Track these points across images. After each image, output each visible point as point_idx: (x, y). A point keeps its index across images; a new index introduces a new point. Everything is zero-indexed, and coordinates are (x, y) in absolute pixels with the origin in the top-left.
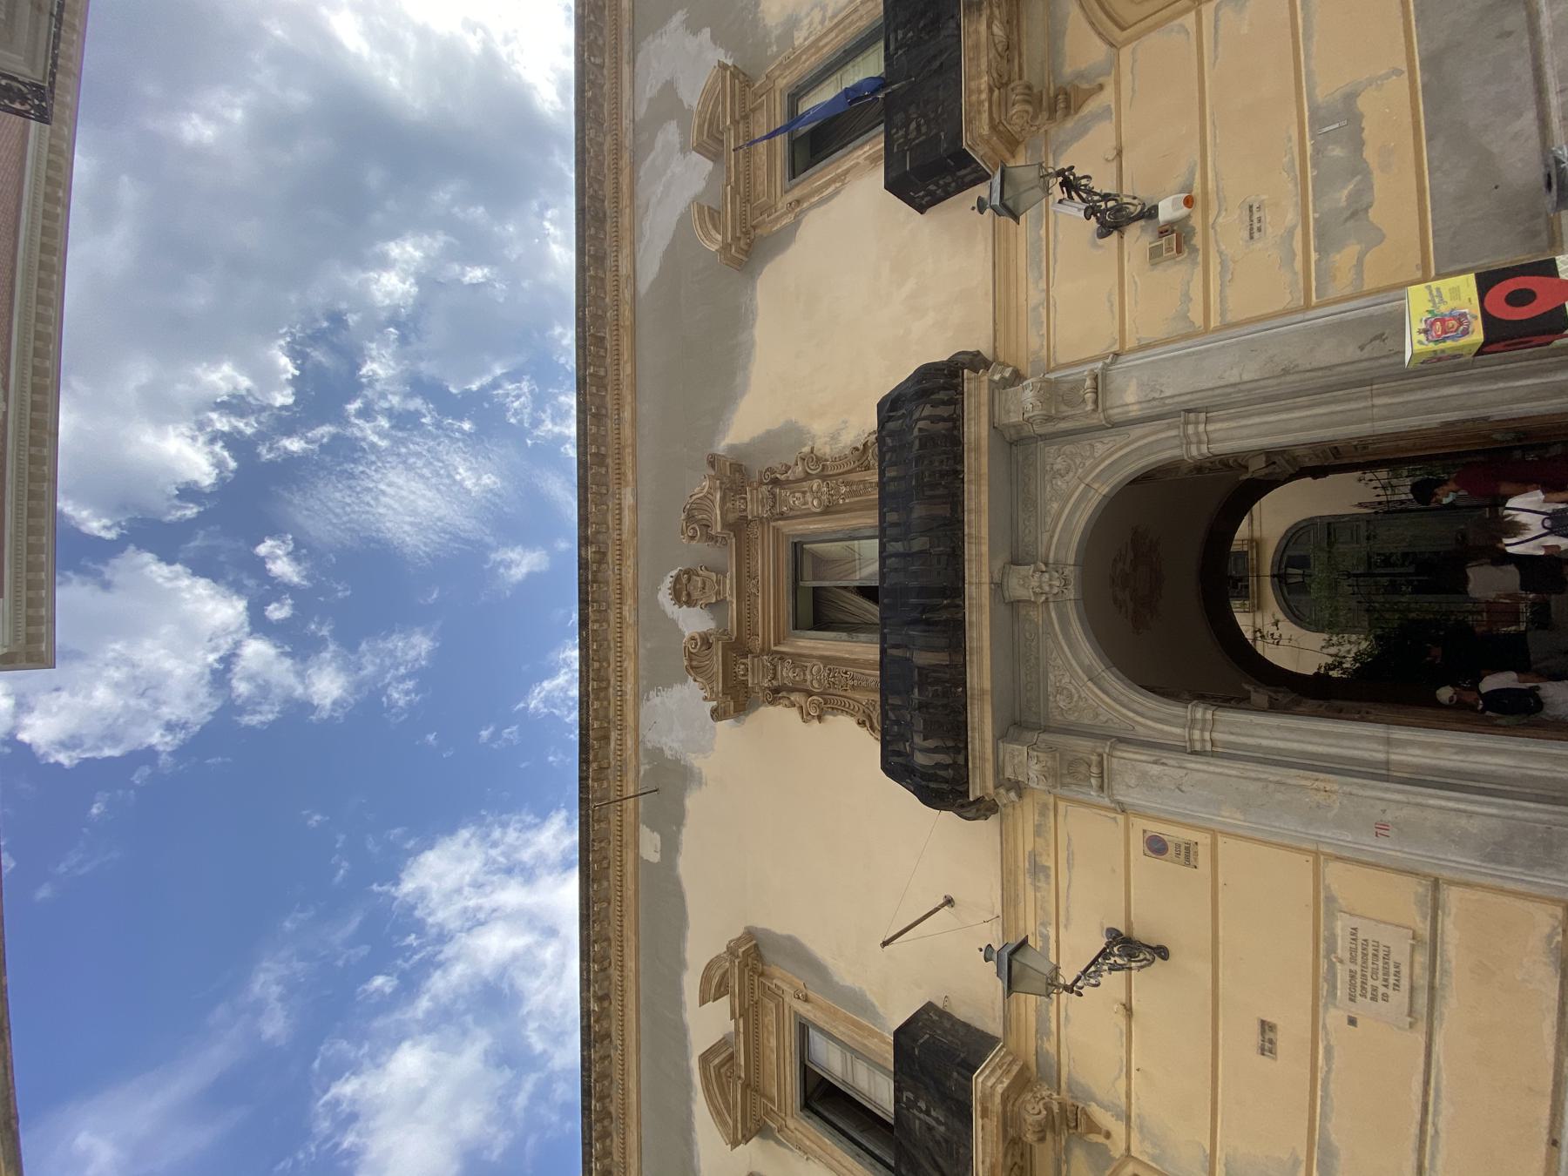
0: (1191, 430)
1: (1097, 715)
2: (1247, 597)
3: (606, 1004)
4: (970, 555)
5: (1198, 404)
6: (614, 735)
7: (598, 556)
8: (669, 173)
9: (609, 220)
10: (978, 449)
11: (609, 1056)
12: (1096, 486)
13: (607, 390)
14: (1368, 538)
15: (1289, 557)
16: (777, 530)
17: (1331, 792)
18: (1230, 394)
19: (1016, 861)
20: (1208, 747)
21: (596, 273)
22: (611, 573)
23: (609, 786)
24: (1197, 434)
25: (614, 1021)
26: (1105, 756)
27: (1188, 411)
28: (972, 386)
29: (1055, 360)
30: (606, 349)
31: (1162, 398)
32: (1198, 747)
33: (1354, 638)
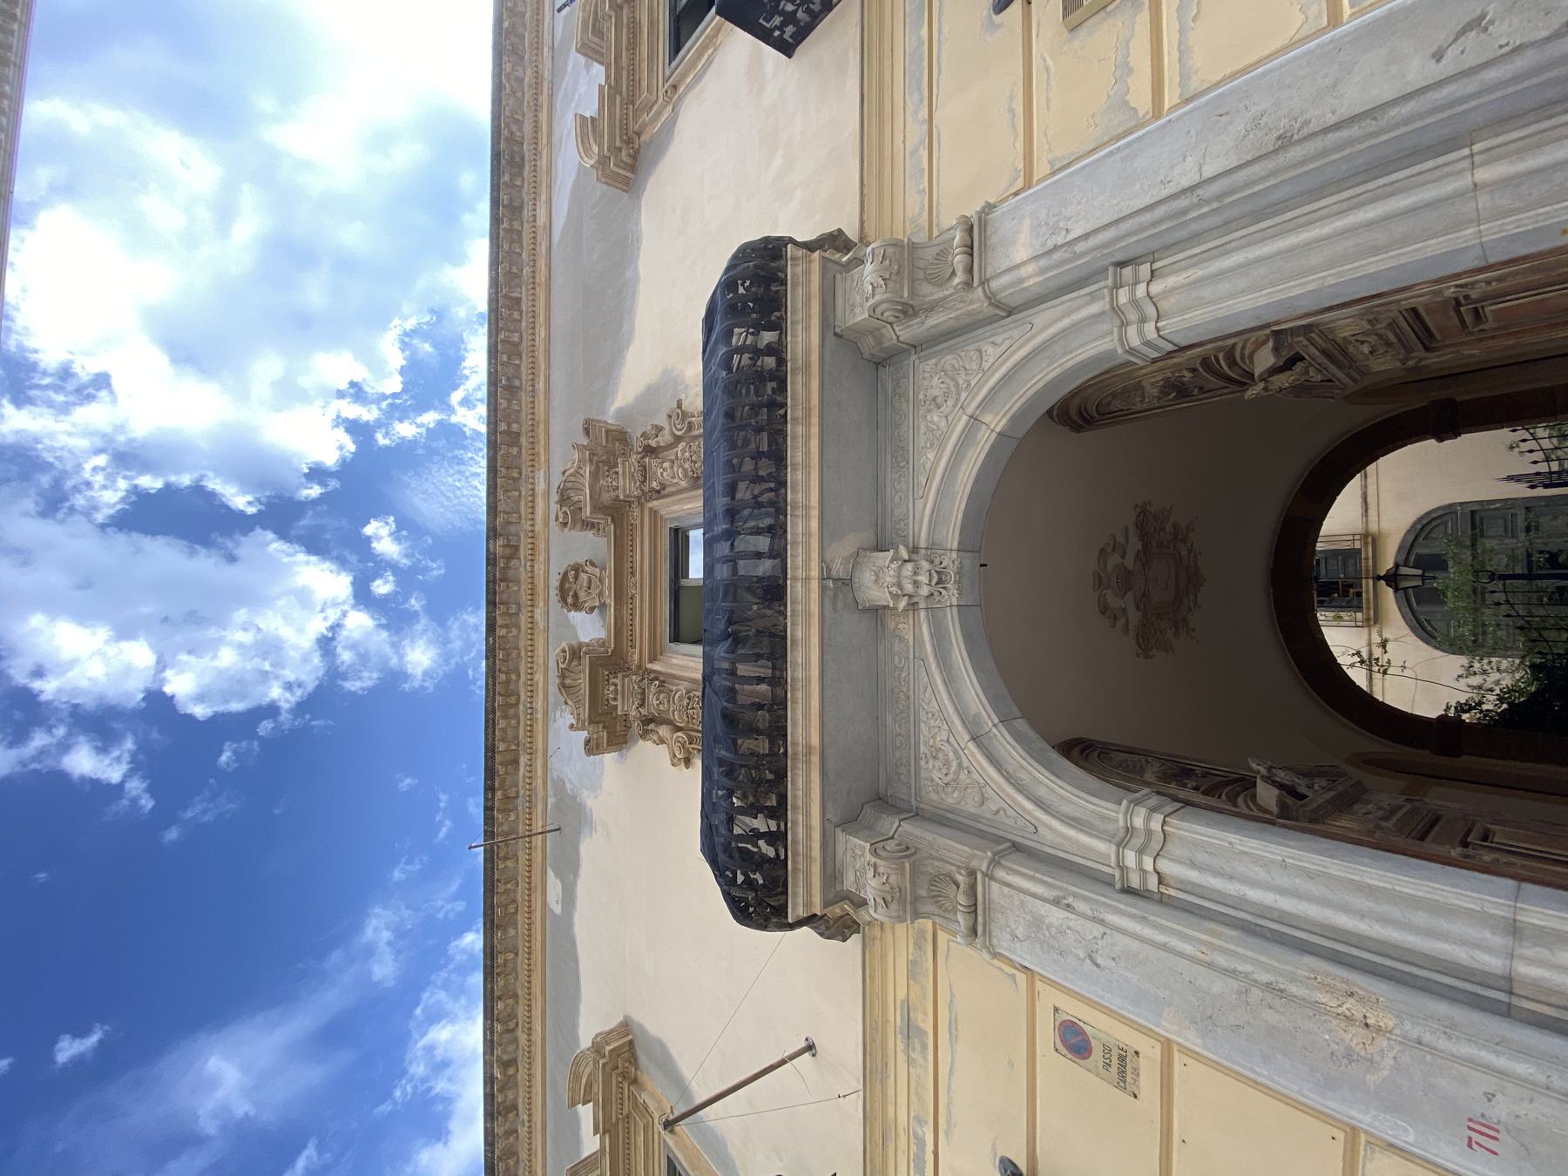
0: (1123, 296)
1: (983, 800)
2: (1359, 608)
3: (511, 1071)
4: (795, 535)
5: (1139, 250)
6: (523, 760)
7: (508, 551)
8: (577, 97)
9: (527, 164)
10: (807, 367)
11: (516, 1131)
12: (987, 418)
13: (521, 358)
14: (1528, 530)
15: (1418, 556)
16: (654, 513)
17: (1379, 1030)
18: (1184, 212)
19: (884, 1011)
20: (1153, 883)
21: (510, 225)
22: (522, 569)
23: (517, 817)
24: (1134, 302)
25: (520, 1090)
26: (979, 876)
27: (1121, 264)
28: (799, 269)
29: (938, 225)
30: (522, 312)
31: (1069, 243)
32: (1135, 881)
33: (1505, 664)
